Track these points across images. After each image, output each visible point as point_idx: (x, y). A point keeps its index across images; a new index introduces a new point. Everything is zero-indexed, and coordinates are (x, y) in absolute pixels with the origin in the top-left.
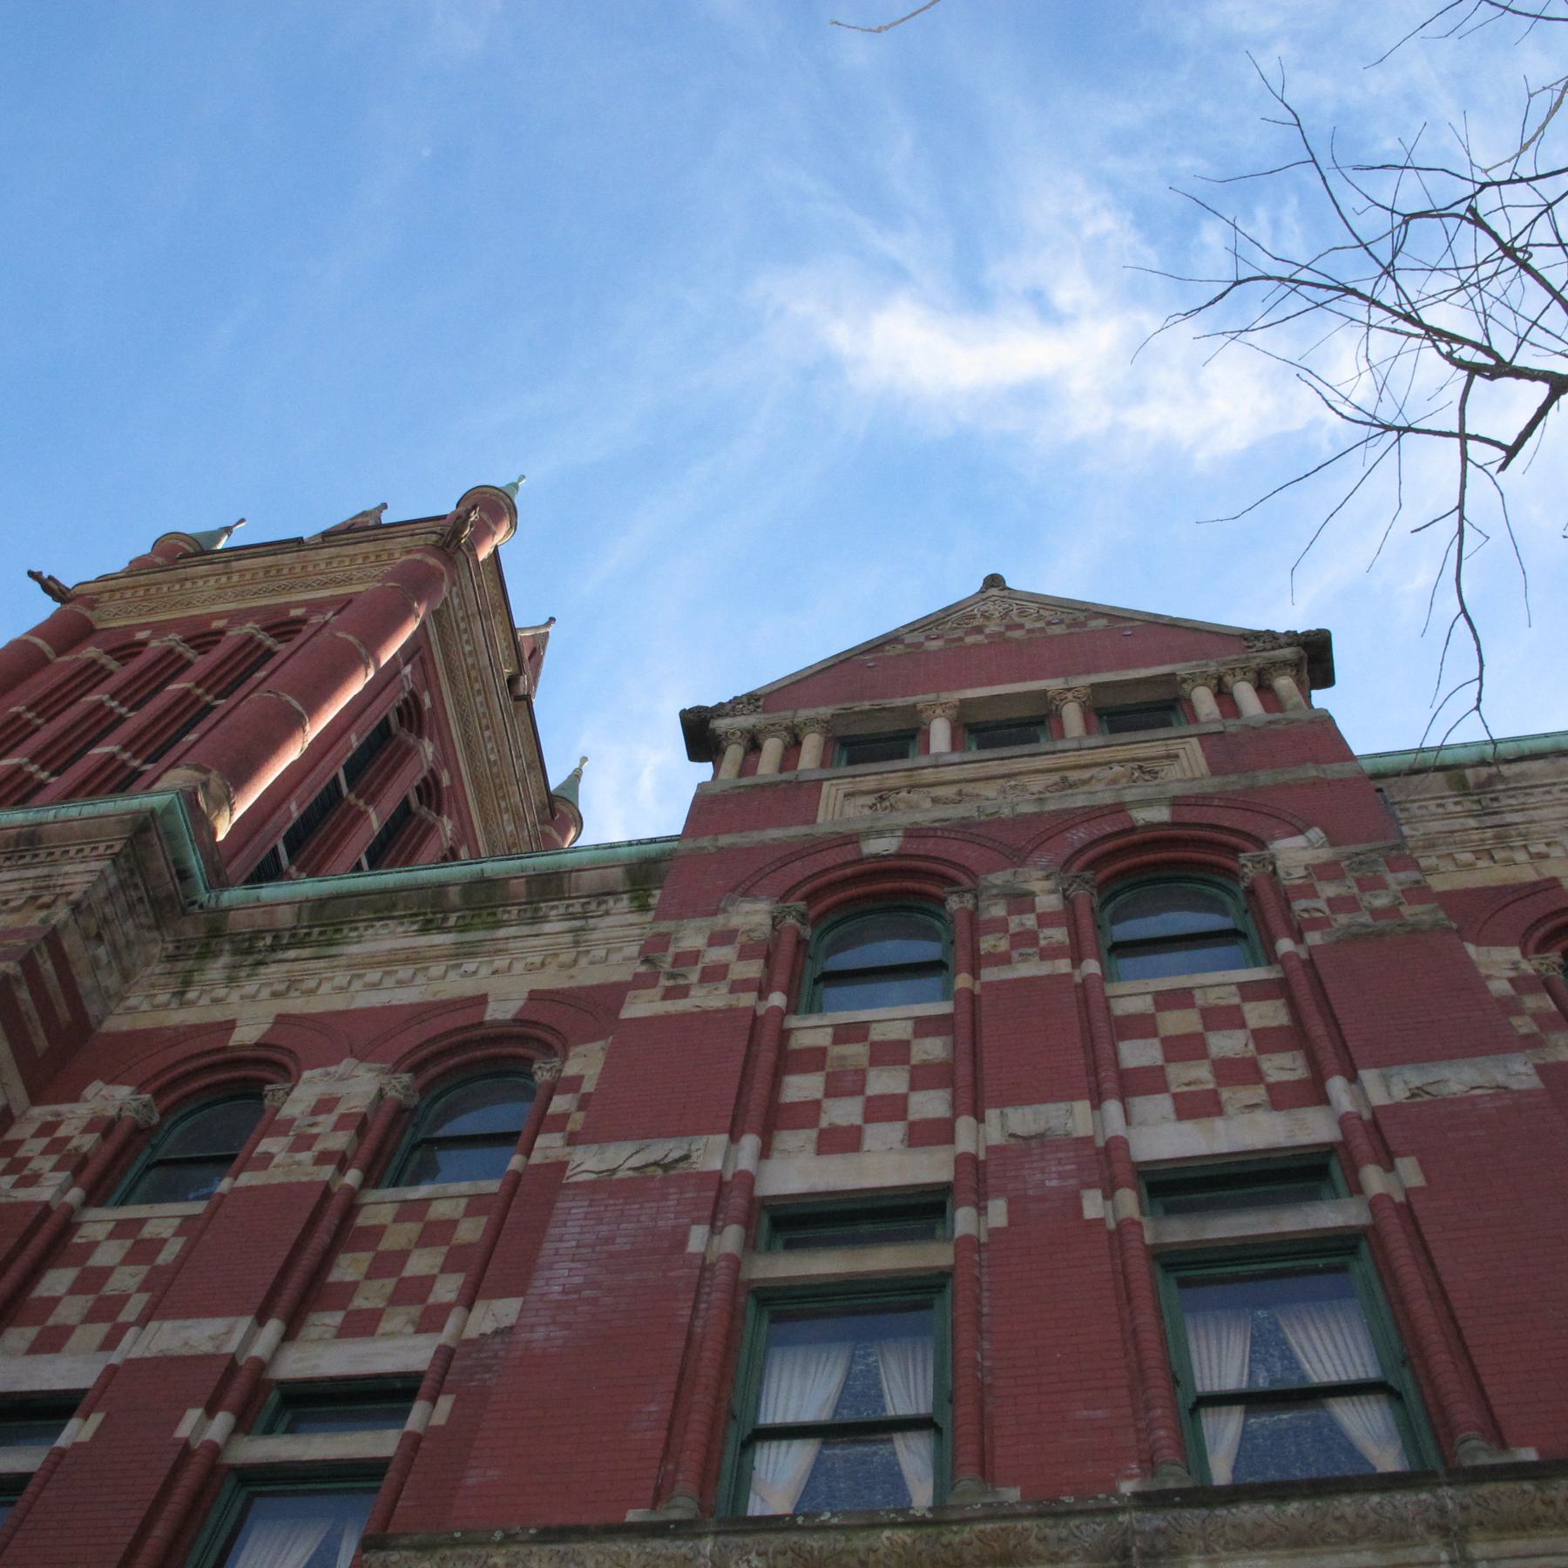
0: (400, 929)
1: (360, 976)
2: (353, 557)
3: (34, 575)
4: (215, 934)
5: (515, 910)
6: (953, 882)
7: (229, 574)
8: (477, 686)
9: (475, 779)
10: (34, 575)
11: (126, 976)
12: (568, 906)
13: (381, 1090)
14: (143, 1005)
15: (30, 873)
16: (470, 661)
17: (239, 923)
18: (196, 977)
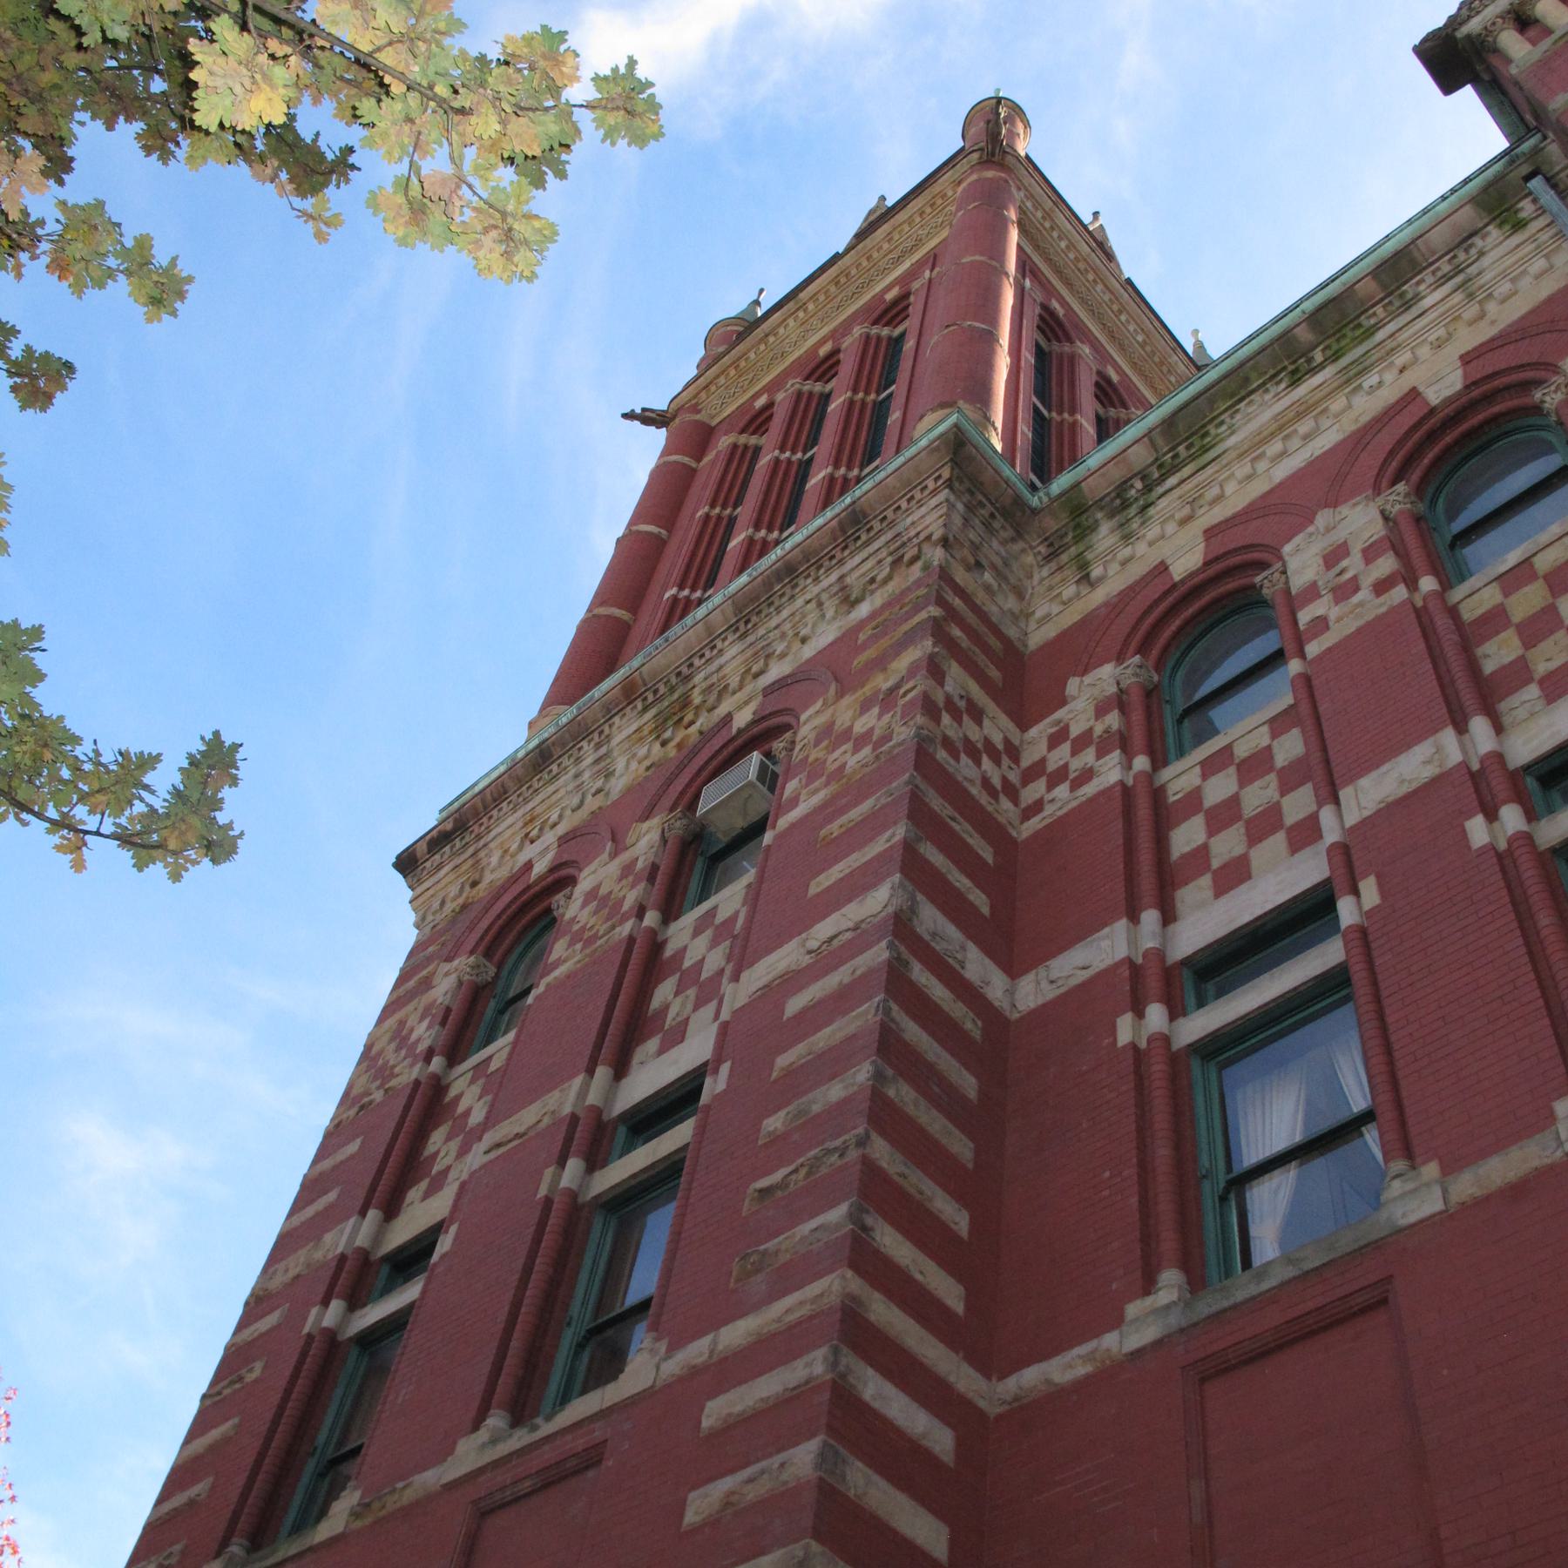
0: (1267, 397)
1: (1262, 455)
2: (910, 221)
3: (629, 416)
4: (1079, 513)
5: (1379, 309)
6: (1538, 383)
7: (803, 307)
8: (1091, 277)
9: (1134, 365)
10: (629, 416)
11: (1020, 594)
12: (1433, 273)
13: (1382, 512)
14: (1051, 608)
15: (876, 545)
16: (1072, 256)
17: (1097, 488)
18: (1089, 556)
